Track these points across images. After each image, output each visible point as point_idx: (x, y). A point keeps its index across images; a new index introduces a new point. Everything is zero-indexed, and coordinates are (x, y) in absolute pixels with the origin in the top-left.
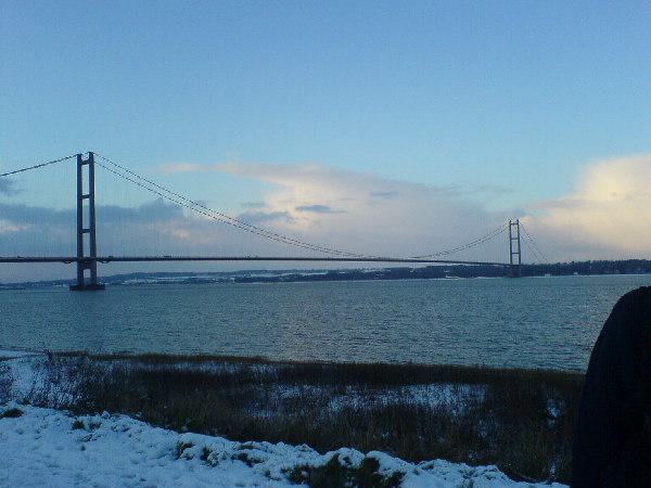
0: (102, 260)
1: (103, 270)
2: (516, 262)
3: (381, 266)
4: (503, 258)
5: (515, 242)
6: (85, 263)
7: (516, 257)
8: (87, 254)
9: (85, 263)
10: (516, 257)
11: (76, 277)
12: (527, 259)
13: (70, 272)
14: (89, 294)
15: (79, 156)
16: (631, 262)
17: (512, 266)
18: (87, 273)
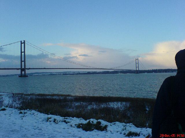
0: (27, 69)
1: (27, 72)
3: (102, 70)
4: (134, 68)
5: (137, 64)
7: (137, 68)
8: (23, 67)
9: (23, 70)
10: (137, 68)
11: (20, 73)
12: (141, 69)
13: (19, 72)
14: (24, 78)
15: (21, 41)
16: (168, 70)
17: (136, 71)
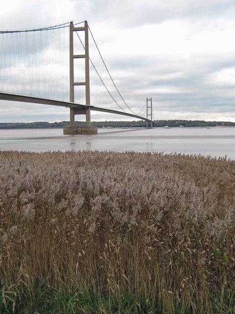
0: (93, 108)
1: (96, 116)
2: (149, 118)
6: (78, 109)
11: (69, 120)
13: (63, 114)
18: (80, 118)
